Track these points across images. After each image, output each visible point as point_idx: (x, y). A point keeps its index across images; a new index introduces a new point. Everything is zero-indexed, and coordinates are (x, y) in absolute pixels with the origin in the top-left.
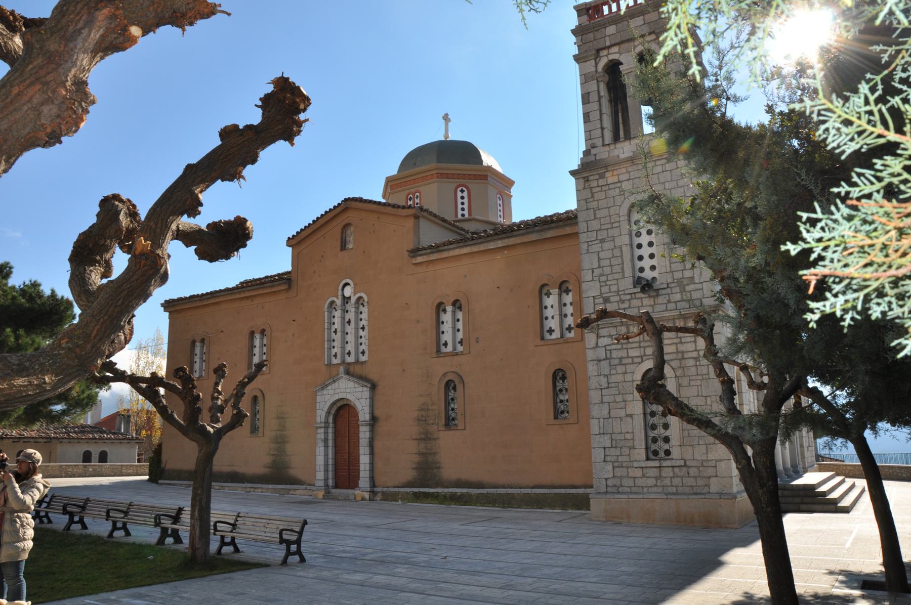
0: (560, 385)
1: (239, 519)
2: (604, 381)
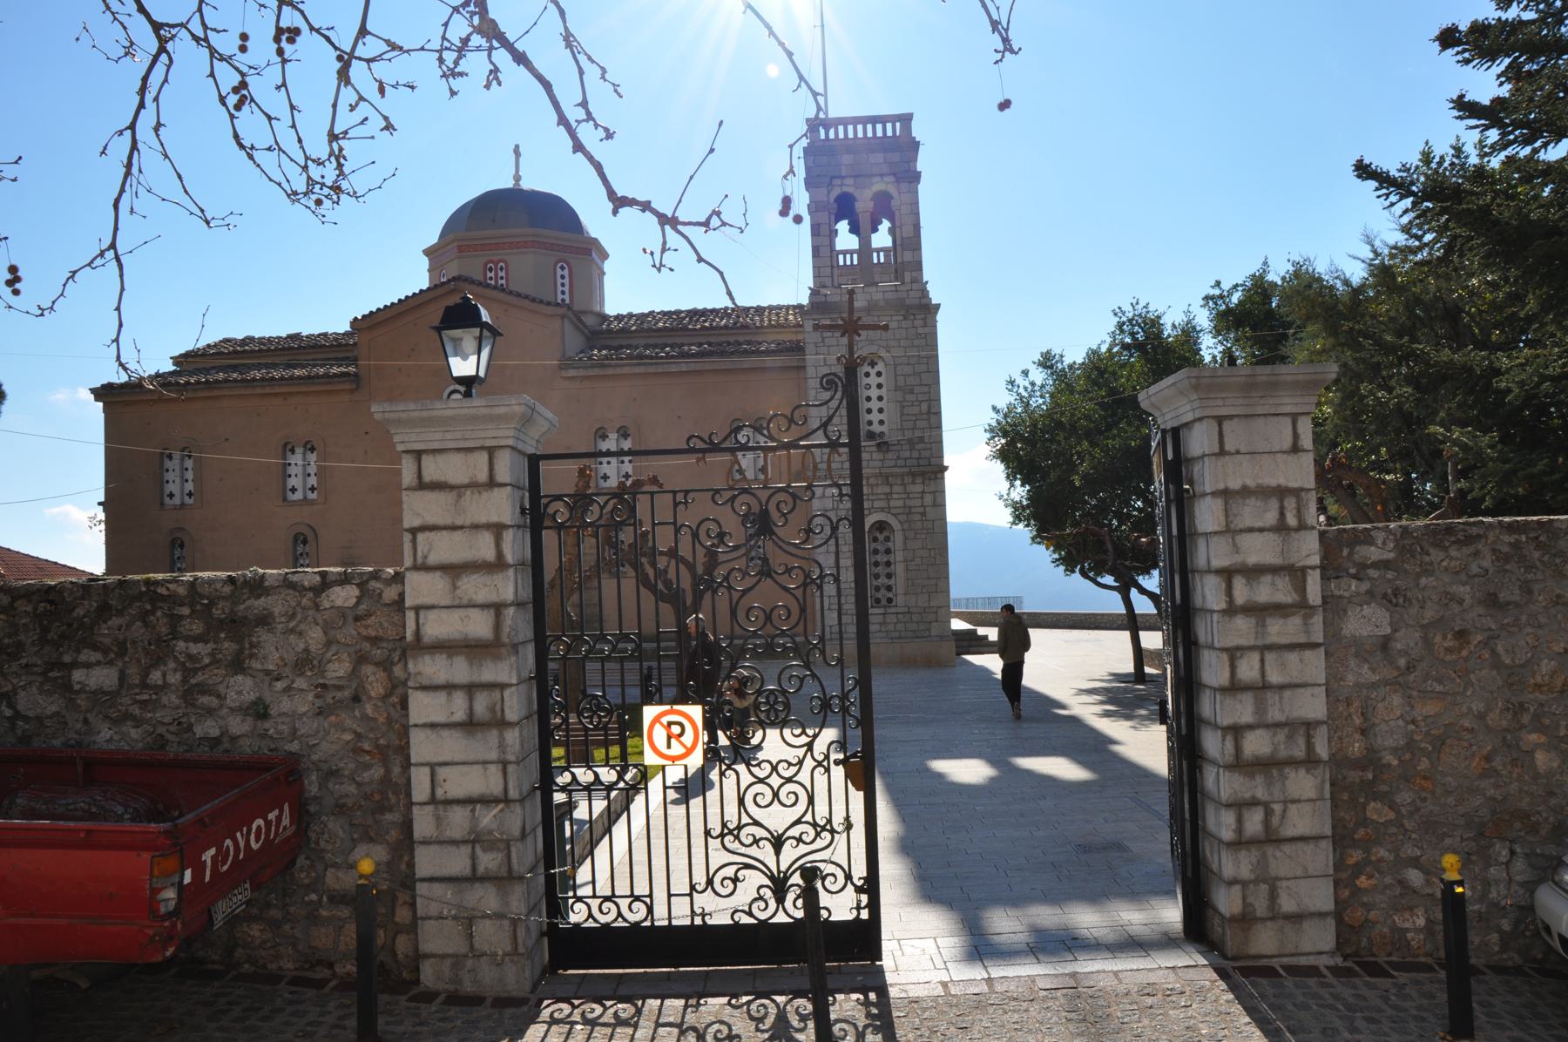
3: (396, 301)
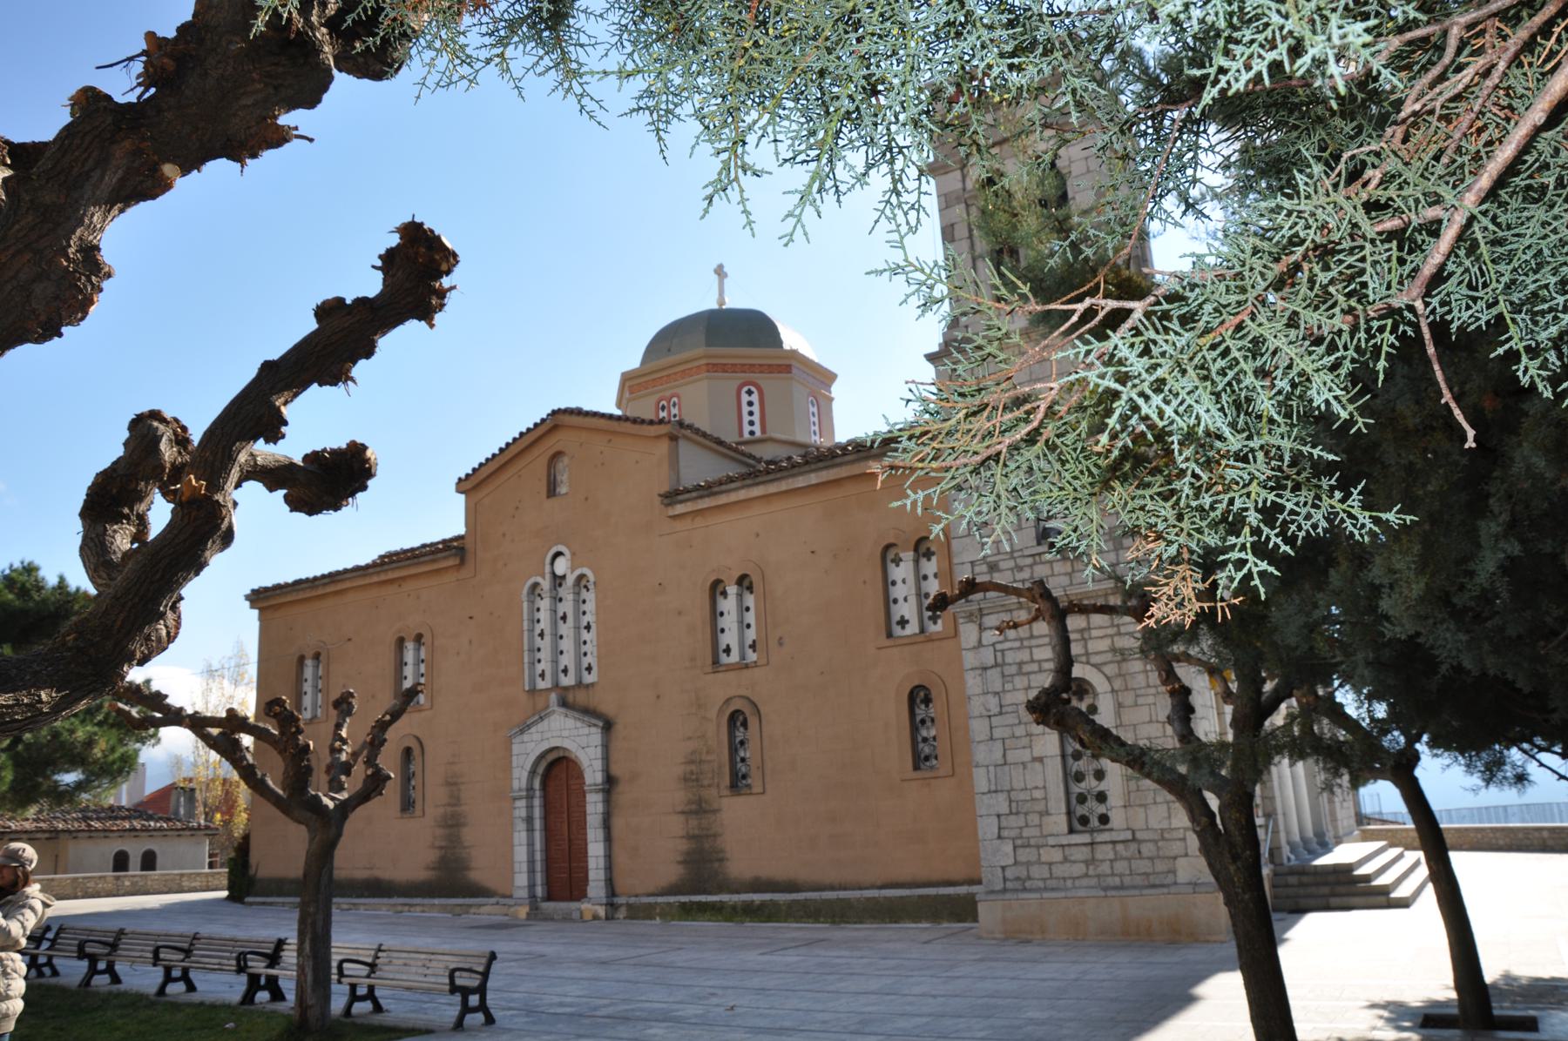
0: (921, 712)
1: (380, 954)
2: (993, 703)
3: (497, 452)
